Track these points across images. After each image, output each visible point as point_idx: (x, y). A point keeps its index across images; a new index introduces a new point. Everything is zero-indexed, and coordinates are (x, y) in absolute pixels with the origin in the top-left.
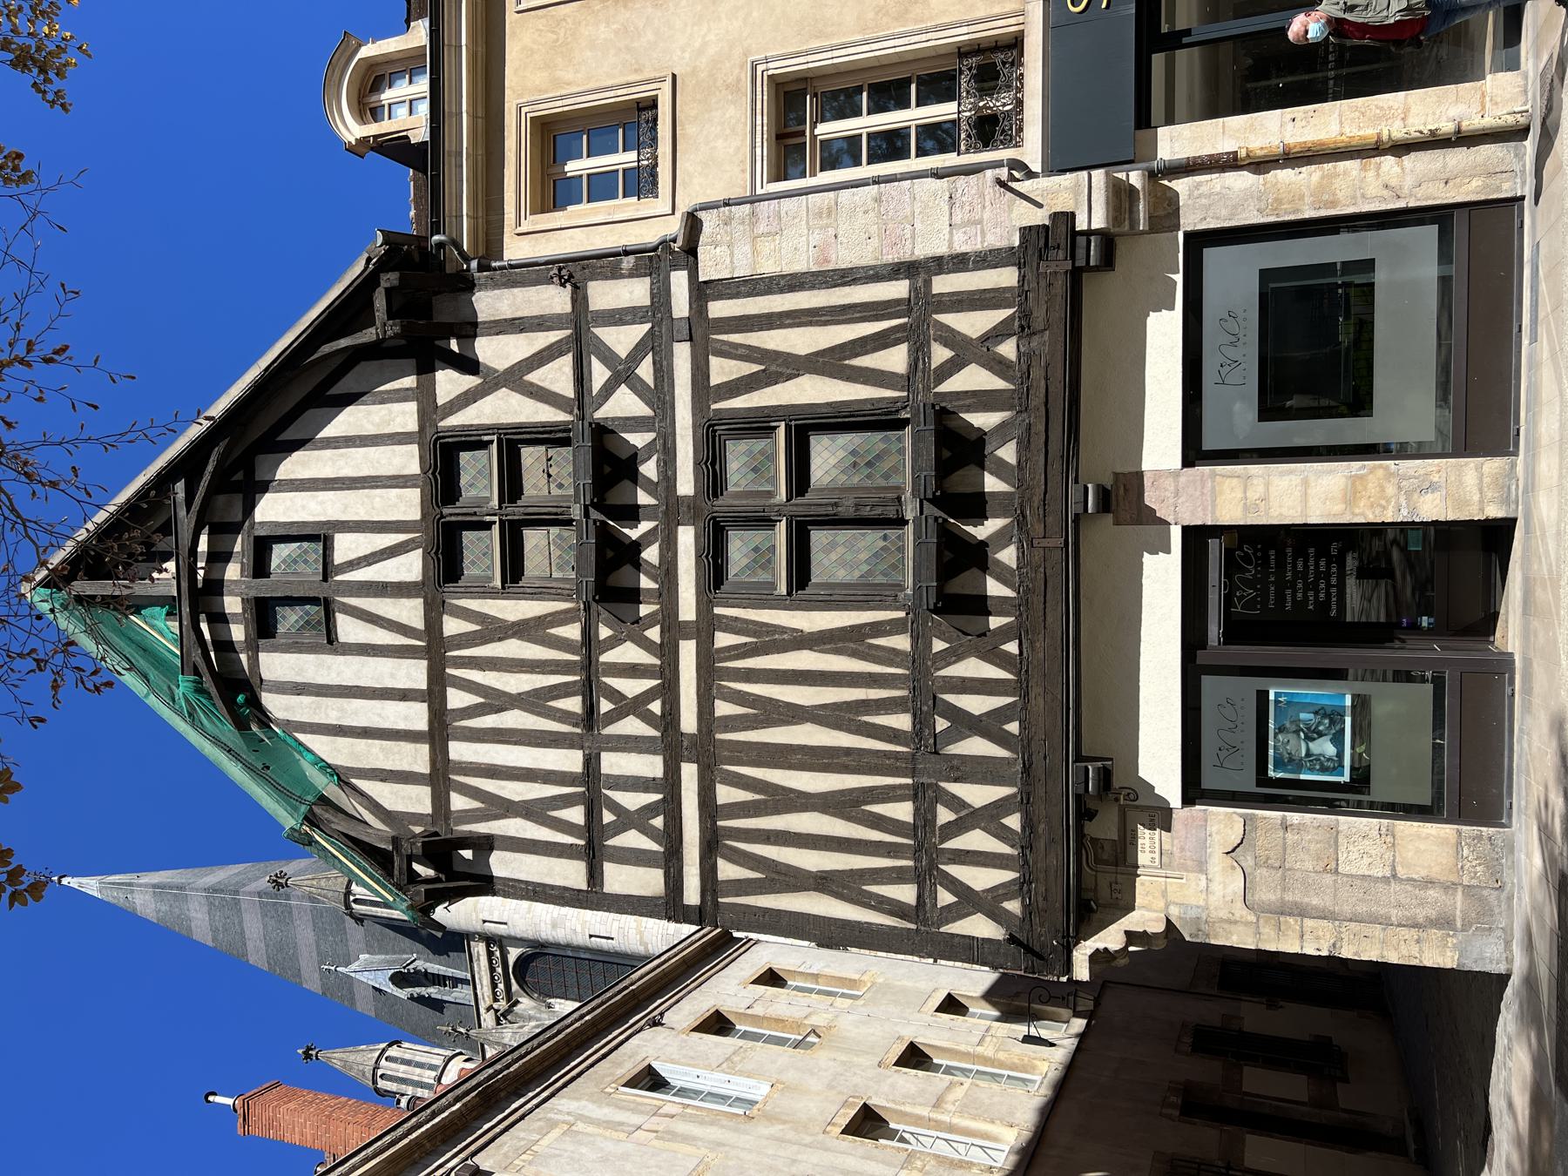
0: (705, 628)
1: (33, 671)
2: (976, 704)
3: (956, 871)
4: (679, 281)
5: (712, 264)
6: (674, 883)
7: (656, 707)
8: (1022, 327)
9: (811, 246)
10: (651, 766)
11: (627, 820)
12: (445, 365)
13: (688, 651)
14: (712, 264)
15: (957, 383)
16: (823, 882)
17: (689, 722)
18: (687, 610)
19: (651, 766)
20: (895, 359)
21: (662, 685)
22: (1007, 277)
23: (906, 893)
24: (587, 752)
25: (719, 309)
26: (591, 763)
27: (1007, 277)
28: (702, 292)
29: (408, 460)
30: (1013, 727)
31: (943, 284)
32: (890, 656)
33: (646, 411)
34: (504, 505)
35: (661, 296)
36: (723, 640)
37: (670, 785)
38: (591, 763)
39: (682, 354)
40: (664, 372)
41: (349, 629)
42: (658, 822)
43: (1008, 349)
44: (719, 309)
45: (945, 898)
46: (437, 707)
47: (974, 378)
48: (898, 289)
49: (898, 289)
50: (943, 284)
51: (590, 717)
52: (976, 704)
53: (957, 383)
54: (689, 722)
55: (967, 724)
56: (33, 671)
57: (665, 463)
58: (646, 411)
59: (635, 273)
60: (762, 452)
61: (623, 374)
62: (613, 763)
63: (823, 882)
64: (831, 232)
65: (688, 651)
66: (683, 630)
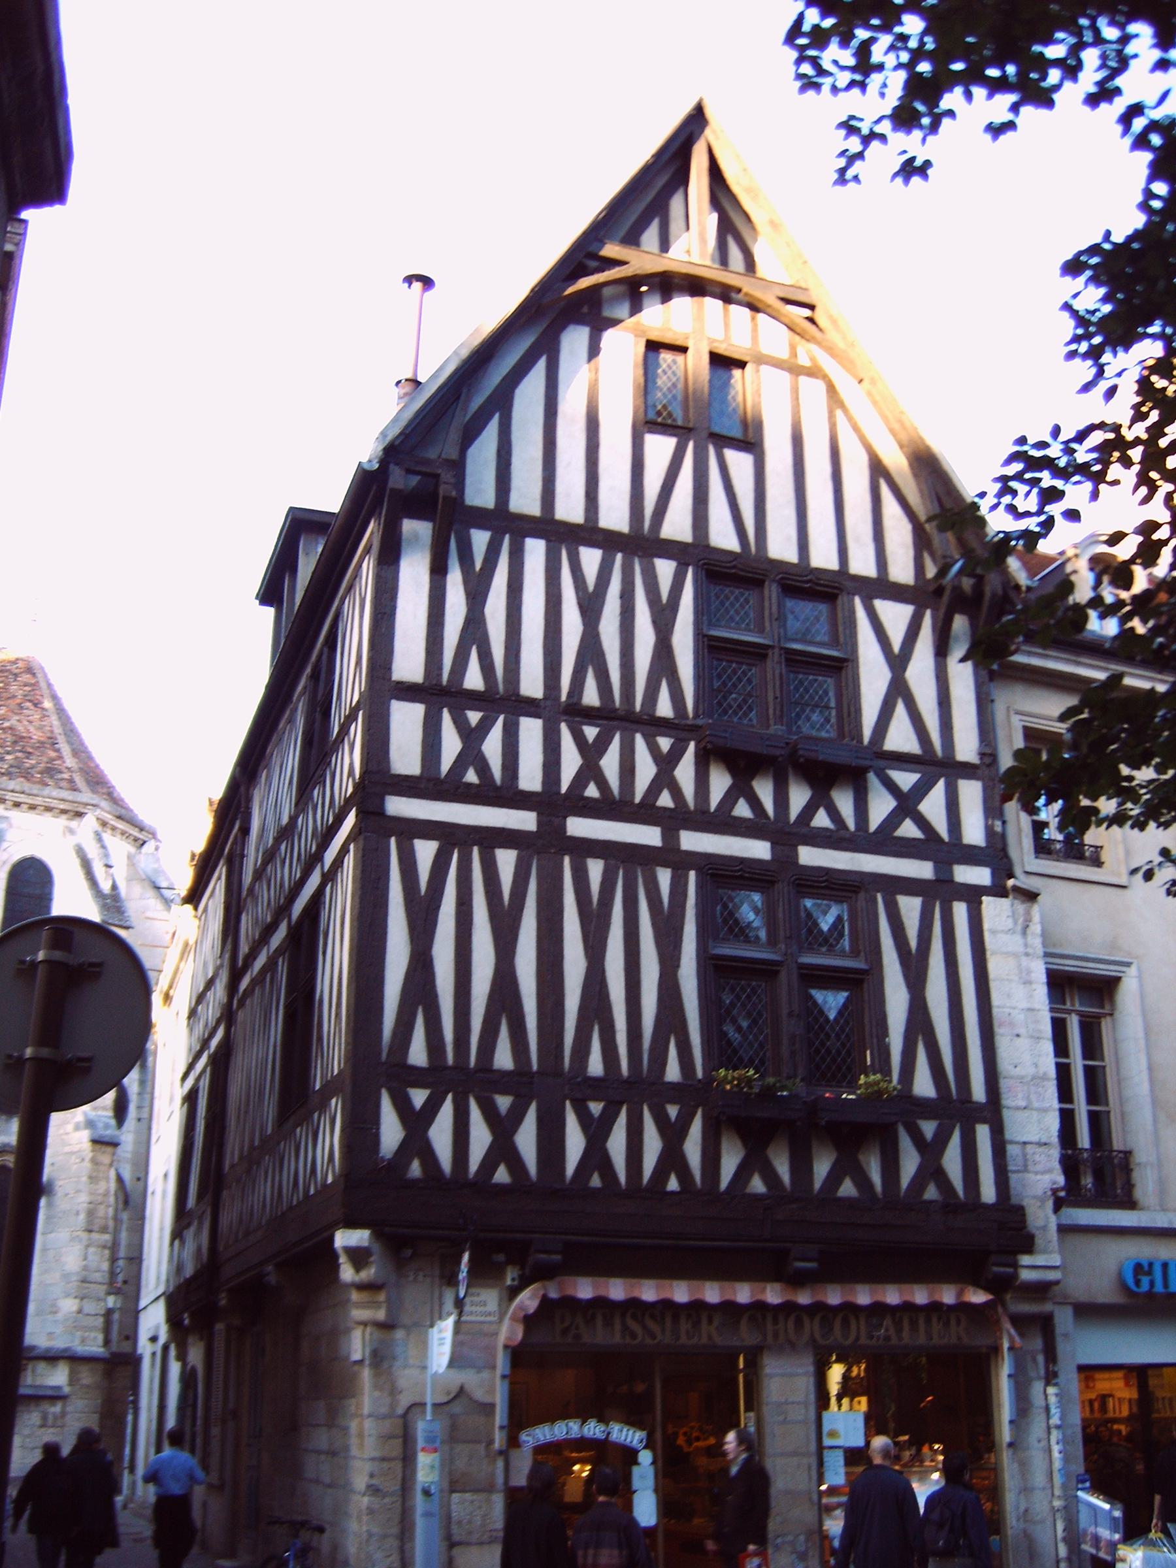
0: (670, 855)
1: (1075, 296)
2: (652, 1145)
3: (447, 1110)
4: (979, 876)
5: (994, 910)
6: (409, 787)
7: (471, 777)
8: (950, 1204)
9: (1011, 1011)
10: (530, 778)
11: (472, 738)
12: (940, 624)
13: (649, 836)
14: (994, 910)
15: (906, 1143)
16: (421, 963)
17: (579, 827)
18: (692, 841)
19: (530, 778)
20: (924, 1085)
21: (688, 812)
22: (988, 1193)
23: (418, 1055)
24: (542, 704)
25: (960, 910)
26: (531, 707)
27: (988, 1193)
28: (973, 895)
29: (823, 557)
30: (596, 1181)
31: (983, 1133)
32: (659, 1060)
33: (873, 825)
34: (706, 639)
35: (972, 856)
36: (664, 877)
37: (508, 796)
38: (531, 707)
39: (922, 870)
40: (906, 849)
41: (660, 448)
42: (471, 777)
43: (931, 1193)
44: (960, 910)
45: (419, 1097)
46: (601, 538)
47: (910, 1163)
48: (979, 1092)
49: (979, 1092)
50: (983, 1133)
51: (577, 713)
52: (652, 1145)
53: (906, 1143)
54: (579, 827)
55: (597, 1133)
56: (1075, 296)
57: (830, 837)
58: (873, 825)
59: (989, 832)
60: (757, 937)
61: (907, 804)
62: (531, 730)
63: (421, 963)
64: (1022, 1031)
65: (649, 836)
66: (944, 864)
